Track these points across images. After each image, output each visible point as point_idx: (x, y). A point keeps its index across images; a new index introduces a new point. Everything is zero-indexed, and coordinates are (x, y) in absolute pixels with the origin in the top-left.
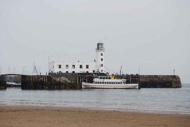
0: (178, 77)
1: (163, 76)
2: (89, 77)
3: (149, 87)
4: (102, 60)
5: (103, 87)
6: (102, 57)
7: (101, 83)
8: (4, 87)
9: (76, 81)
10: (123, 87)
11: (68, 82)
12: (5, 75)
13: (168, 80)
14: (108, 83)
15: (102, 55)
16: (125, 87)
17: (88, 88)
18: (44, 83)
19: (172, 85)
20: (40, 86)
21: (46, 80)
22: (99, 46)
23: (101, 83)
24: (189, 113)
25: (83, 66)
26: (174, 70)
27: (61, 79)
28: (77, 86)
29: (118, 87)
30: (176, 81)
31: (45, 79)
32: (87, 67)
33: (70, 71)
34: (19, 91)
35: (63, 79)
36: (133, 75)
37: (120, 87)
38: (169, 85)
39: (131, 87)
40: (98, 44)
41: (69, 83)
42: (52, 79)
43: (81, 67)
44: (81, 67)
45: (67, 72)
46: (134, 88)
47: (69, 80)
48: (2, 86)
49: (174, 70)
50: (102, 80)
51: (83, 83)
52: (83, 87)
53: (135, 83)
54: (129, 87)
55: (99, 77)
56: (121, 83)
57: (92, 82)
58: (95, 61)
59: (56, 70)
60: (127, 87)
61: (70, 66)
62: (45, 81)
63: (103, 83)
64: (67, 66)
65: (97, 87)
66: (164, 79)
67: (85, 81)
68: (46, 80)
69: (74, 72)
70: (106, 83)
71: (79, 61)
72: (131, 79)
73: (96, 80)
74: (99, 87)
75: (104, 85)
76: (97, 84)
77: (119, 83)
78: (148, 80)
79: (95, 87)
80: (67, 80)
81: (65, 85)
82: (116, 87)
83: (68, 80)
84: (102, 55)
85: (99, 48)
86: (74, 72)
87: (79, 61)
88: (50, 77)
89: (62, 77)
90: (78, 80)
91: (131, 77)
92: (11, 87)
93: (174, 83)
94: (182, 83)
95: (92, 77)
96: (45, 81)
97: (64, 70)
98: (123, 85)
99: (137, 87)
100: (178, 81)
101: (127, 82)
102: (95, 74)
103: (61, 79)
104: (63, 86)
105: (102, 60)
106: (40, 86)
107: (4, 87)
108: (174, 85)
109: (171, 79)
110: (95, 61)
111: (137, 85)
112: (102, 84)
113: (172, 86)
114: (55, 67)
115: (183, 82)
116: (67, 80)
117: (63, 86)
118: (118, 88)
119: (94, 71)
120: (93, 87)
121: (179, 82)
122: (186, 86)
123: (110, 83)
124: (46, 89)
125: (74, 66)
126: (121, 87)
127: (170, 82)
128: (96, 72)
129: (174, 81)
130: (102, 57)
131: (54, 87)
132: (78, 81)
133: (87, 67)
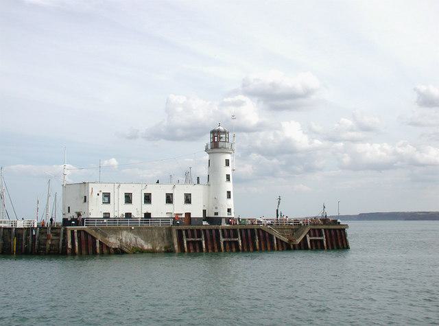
25: (123, 199)
31: (69, 241)
32: (188, 199)
33: (138, 209)
40: (216, 133)
42: (94, 239)
43: (169, 199)
44: (169, 199)
49: (280, 199)
58: (69, 208)
59: (96, 210)
61: (138, 198)
62: (70, 246)
64: (107, 195)
71: (158, 182)
83: (142, 242)
85: (221, 144)
86: (107, 216)
87: (158, 182)
88: (85, 232)
89: (125, 233)
90: (175, 240)
92: (255, 250)
95: (217, 230)
96: (70, 246)
110: (69, 208)
114: (90, 199)
119: (204, 212)
125: (107, 195)
128: (210, 214)
133: (188, 199)
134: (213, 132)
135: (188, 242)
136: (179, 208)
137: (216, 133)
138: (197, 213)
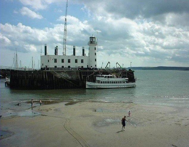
18: (44, 79)
21: (46, 76)
43: (76, 61)
44: (76, 61)
45: (56, 67)
50: (107, 79)
51: (88, 83)
52: (87, 87)
57: (94, 81)
61: (66, 61)
62: (44, 77)
63: (108, 82)
66: (16, 91)
68: (46, 76)
69: (56, 66)
85: (93, 42)
96: (44, 77)
98: (126, 84)
118: (126, 88)
133: (82, 61)
134: (90, 38)
135: (83, 76)
136: (79, 65)
137: (92, 38)
138: (85, 67)
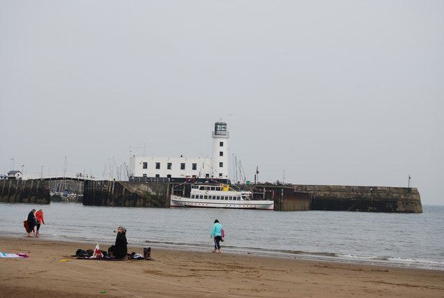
0: (417, 191)
1: (387, 189)
2: (183, 186)
3: (353, 210)
4: (221, 154)
5: (205, 205)
6: (222, 149)
7: (201, 197)
8: (44, 200)
9: (166, 192)
10: (242, 206)
11: (152, 194)
12: (53, 179)
13: (390, 197)
14: (214, 198)
15: (221, 144)
16: (246, 206)
17: (179, 206)
19: (397, 207)
20: (103, 201)
22: (219, 129)
23: (201, 197)
24: (442, 269)
26: (410, 178)
27: (139, 189)
28: (165, 203)
29: (232, 206)
30: (406, 200)
32: (194, 167)
33: (163, 173)
34: (79, 209)
35: (144, 188)
36: (271, 184)
37: (236, 206)
38: (391, 206)
39: (257, 207)
41: (153, 197)
43: (183, 166)
44: (183, 166)
45: (158, 176)
46: (264, 209)
47: (153, 191)
48: (42, 198)
50: (203, 193)
51: (173, 197)
52: (172, 204)
53: (94, 183)
54: (253, 206)
55: (199, 186)
56: (239, 198)
57: (188, 195)
59: (139, 172)
60: (249, 206)
63: (206, 197)
65: (194, 204)
66: (383, 195)
67: (175, 193)
70: (210, 197)
72: (259, 191)
73: (194, 191)
74: (198, 205)
75: (228, 201)
76: (195, 200)
77: (235, 199)
78: (352, 196)
79: (190, 204)
80: (150, 190)
81: (144, 199)
82: (228, 206)
83: (151, 191)
84: (221, 144)
89: (142, 185)
91: (266, 188)
93: (401, 202)
94: (422, 204)
97: (151, 172)
98: (242, 201)
99: (272, 207)
100: (416, 200)
101: (256, 197)
102: (210, 180)
103: (139, 189)
104: (140, 201)
105: (221, 154)
106: (103, 201)
107: (44, 200)
108: (401, 208)
109: (395, 195)
111: (273, 202)
112: (203, 200)
113: (397, 210)
115: (425, 201)
116: (150, 190)
117: (140, 201)
119: (207, 175)
120: (187, 204)
121: (418, 202)
122: (435, 209)
123: (222, 198)
124: (111, 206)
126: (238, 206)
127: (397, 201)
129: (402, 200)
130: (222, 149)
131: (124, 203)
132: (162, 193)
133: (194, 167)
